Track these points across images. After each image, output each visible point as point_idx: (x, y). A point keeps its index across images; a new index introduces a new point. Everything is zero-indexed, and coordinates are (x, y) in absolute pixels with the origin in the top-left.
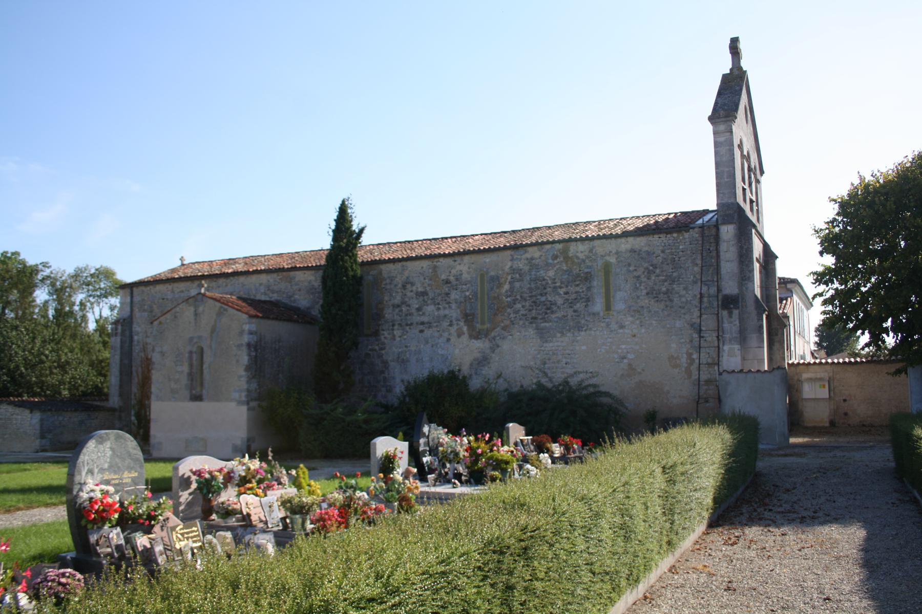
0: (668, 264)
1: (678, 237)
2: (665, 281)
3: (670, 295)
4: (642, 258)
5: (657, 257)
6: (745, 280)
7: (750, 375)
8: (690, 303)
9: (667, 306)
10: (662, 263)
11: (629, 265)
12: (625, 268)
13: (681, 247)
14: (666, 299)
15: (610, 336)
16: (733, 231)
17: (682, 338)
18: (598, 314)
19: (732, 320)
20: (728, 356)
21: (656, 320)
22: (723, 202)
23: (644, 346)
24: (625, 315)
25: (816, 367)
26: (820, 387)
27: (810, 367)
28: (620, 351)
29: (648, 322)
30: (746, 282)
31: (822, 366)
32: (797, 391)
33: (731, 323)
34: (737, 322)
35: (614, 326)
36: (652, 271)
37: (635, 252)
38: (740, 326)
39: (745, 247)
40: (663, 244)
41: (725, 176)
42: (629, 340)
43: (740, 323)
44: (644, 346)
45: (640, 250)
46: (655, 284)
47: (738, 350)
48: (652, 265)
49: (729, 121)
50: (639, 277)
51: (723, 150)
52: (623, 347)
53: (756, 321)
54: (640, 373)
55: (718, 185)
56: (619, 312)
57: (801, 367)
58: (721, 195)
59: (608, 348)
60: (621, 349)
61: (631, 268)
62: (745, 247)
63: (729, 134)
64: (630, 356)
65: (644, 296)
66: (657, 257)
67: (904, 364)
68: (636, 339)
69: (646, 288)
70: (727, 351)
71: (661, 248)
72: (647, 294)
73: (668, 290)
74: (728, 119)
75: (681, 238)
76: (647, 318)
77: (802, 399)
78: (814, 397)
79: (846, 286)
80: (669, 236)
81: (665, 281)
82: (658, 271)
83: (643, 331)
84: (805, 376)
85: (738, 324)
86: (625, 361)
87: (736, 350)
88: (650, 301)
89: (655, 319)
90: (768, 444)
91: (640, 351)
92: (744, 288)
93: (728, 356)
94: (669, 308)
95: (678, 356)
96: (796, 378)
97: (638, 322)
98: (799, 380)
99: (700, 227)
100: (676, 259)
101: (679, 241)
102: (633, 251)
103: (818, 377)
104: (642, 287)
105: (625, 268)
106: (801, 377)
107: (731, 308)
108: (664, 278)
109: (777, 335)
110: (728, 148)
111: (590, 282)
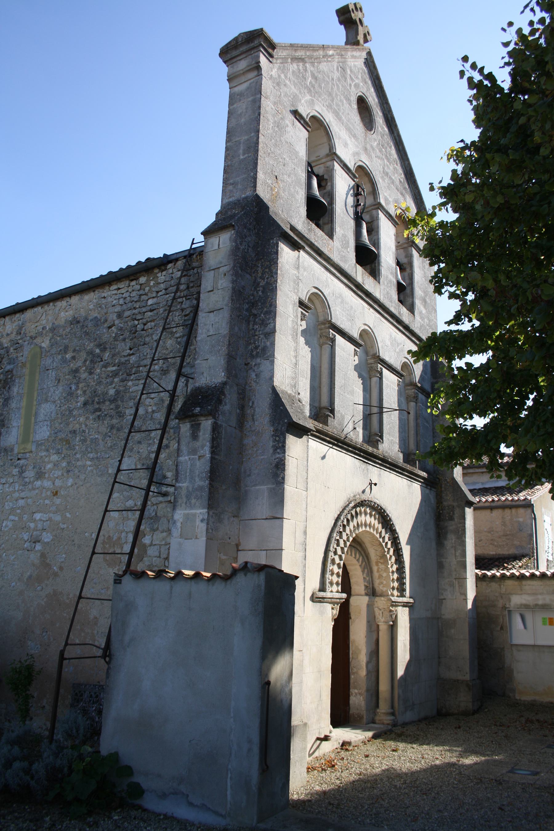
0: (124, 340)
1: (148, 281)
2: (115, 374)
3: (119, 402)
4: (87, 334)
5: (110, 327)
6: (257, 355)
7: (180, 587)
8: (152, 419)
9: (112, 427)
10: (115, 339)
11: (66, 349)
12: (60, 357)
13: (150, 302)
14: (113, 412)
15: (23, 495)
16: (228, 243)
17: (131, 498)
18: (12, 450)
19: (198, 444)
20: (181, 536)
21: (92, 459)
22: (231, 200)
23: (68, 515)
24: (47, 450)
25: (535, 583)
26: (544, 624)
27: (524, 582)
28: (32, 525)
29: (79, 463)
30: (258, 360)
31: (548, 582)
32: (502, 628)
33: (194, 451)
34: (206, 451)
35: (30, 474)
36: (99, 356)
37: (78, 322)
38: (212, 458)
39: (262, 283)
40: (121, 301)
41: (241, 151)
42: (47, 502)
43: (213, 453)
44: (68, 515)
45: (86, 319)
46: (99, 383)
47: (202, 521)
48: (99, 346)
49: (254, 48)
50: (76, 371)
51: (242, 106)
52: (38, 516)
53: (271, 451)
54: (56, 575)
55: (227, 171)
56: (39, 445)
57: (509, 583)
58: (231, 187)
59: (17, 519)
60: (35, 521)
61: (68, 356)
62: (262, 283)
63: (255, 73)
64: (47, 537)
65: (79, 408)
66: (110, 327)
67: (92, 468)
68: (58, 501)
69: (84, 392)
70: (179, 524)
71: (118, 309)
72: (85, 404)
73: (118, 392)
74: (252, 45)
75: (152, 283)
76: (78, 456)
77: (512, 645)
78: (532, 643)
79: (538, 389)
80: (133, 283)
81: (115, 374)
82: (106, 355)
83: (70, 482)
84: (516, 600)
85: (208, 456)
86: (38, 547)
87: (198, 522)
88: (87, 418)
89: (91, 455)
90: (204, 807)
91: (62, 526)
92: (253, 375)
93: (181, 536)
94: (115, 431)
95: (119, 538)
96: (500, 604)
97: (64, 464)
98: (504, 608)
99: (185, 257)
100: (139, 327)
101: (147, 289)
102: (75, 321)
103: (540, 602)
104: (79, 392)
105: (60, 357)
106: (510, 601)
107: (197, 415)
108: (114, 368)
109: (451, 519)
110: (251, 99)
111: (9, 388)
